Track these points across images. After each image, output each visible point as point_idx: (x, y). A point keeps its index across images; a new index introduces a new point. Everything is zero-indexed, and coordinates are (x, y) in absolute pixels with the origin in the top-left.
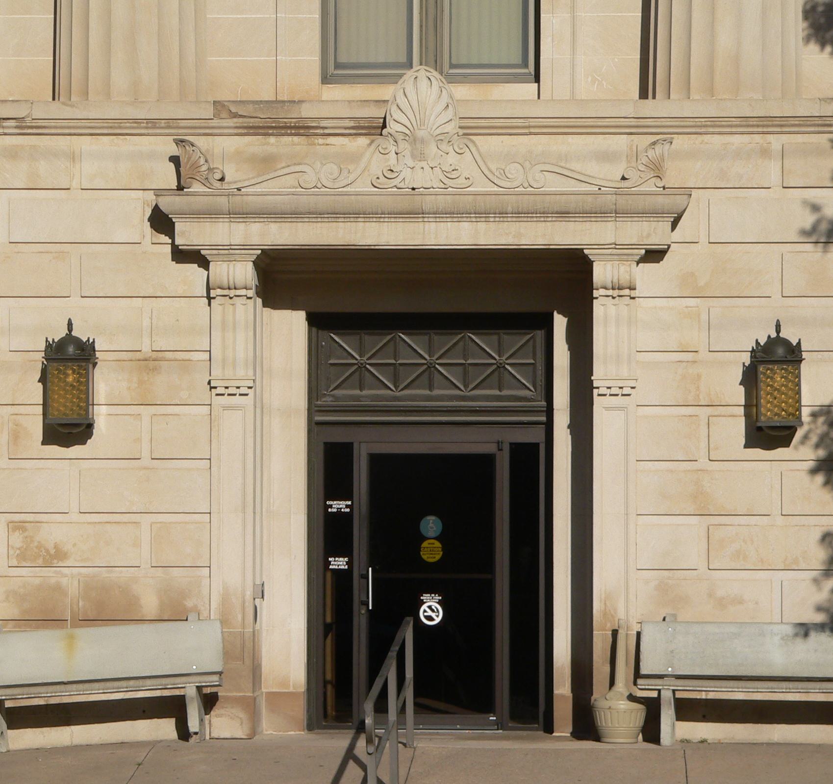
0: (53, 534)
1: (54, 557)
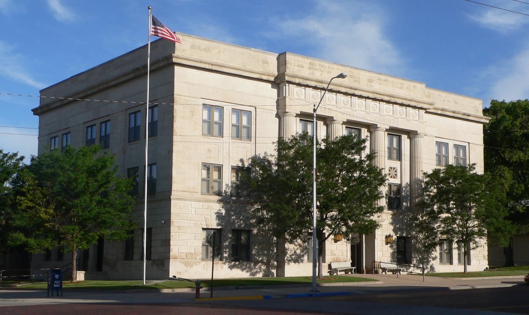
0: (335, 252)
1: (335, 255)
